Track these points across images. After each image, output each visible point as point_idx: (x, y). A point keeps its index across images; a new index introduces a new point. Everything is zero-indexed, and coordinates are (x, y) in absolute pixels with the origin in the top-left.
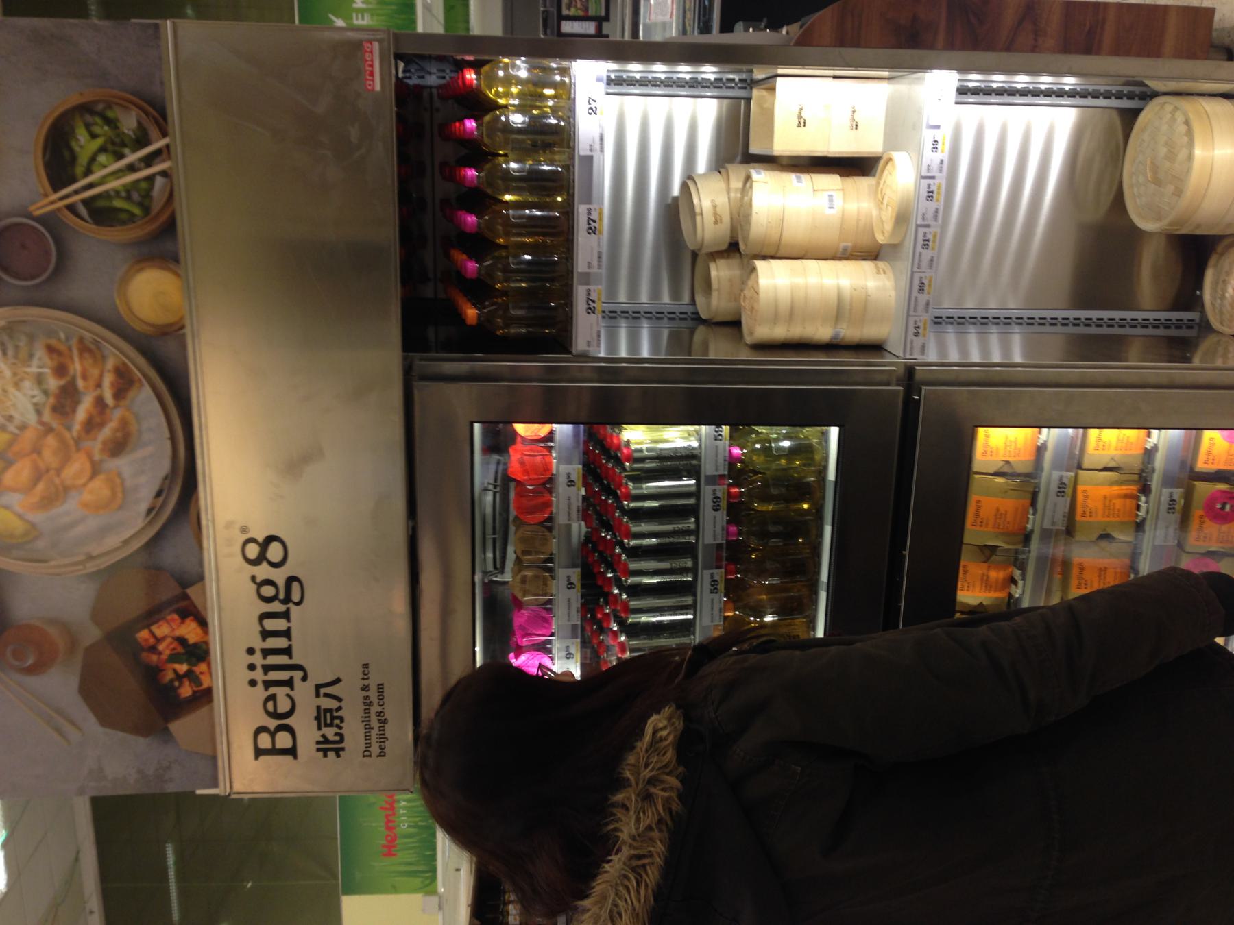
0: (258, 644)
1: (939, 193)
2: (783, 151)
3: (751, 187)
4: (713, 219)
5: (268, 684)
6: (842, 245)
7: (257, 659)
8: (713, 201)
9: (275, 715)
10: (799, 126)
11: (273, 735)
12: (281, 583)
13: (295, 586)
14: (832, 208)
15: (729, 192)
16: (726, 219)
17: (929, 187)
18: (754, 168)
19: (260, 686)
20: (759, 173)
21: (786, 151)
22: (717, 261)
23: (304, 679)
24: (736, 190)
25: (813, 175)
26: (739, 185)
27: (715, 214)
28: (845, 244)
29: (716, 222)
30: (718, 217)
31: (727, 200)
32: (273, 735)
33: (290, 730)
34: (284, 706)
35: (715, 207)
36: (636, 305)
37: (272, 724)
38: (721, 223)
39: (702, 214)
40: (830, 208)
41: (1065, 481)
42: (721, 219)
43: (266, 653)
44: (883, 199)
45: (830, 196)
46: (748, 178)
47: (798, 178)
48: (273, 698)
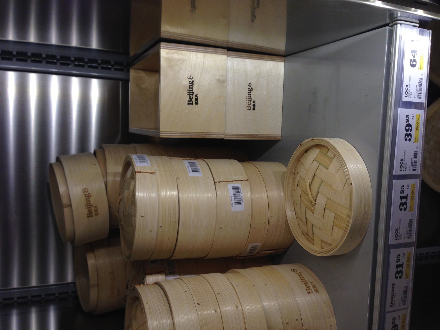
0: (248, 96)
1: (412, 199)
2: (171, 132)
3: (133, 177)
4: (86, 211)
5: (248, 101)
6: (250, 246)
7: (248, 98)
8: (85, 190)
9: (249, 105)
10: (190, 103)
11: (248, 107)
12: (250, 88)
13: (252, 89)
14: (240, 204)
15: (105, 175)
16: (104, 209)
17: (402, 192)
18: (136, 153)
19: (247, 101)
20: (142, 160)
21: (175, 133)
22: (96, 252)
23: (252, 100)
24: (115, 174)
25: (211, 162)
26: (119, 169)
27: (89, 205)
28: (254, 244)
29: (90, 215)
30: (93, 209)
31: (103, 186)
32: (248, 107)
33: (250, 107)
34: (250, 104)
35: (88, 197)
36: (6, 291)
37: (248, 106)
38: (97, 215)
39: (70, 205)
40: (236, 204)
41: (407, 192)
42: (96, 211)
43: (248, 97)
44: (316, 200)
45: (235, 188)
46: (128, 164)
47: (192, 165)
48: (248, 103)
